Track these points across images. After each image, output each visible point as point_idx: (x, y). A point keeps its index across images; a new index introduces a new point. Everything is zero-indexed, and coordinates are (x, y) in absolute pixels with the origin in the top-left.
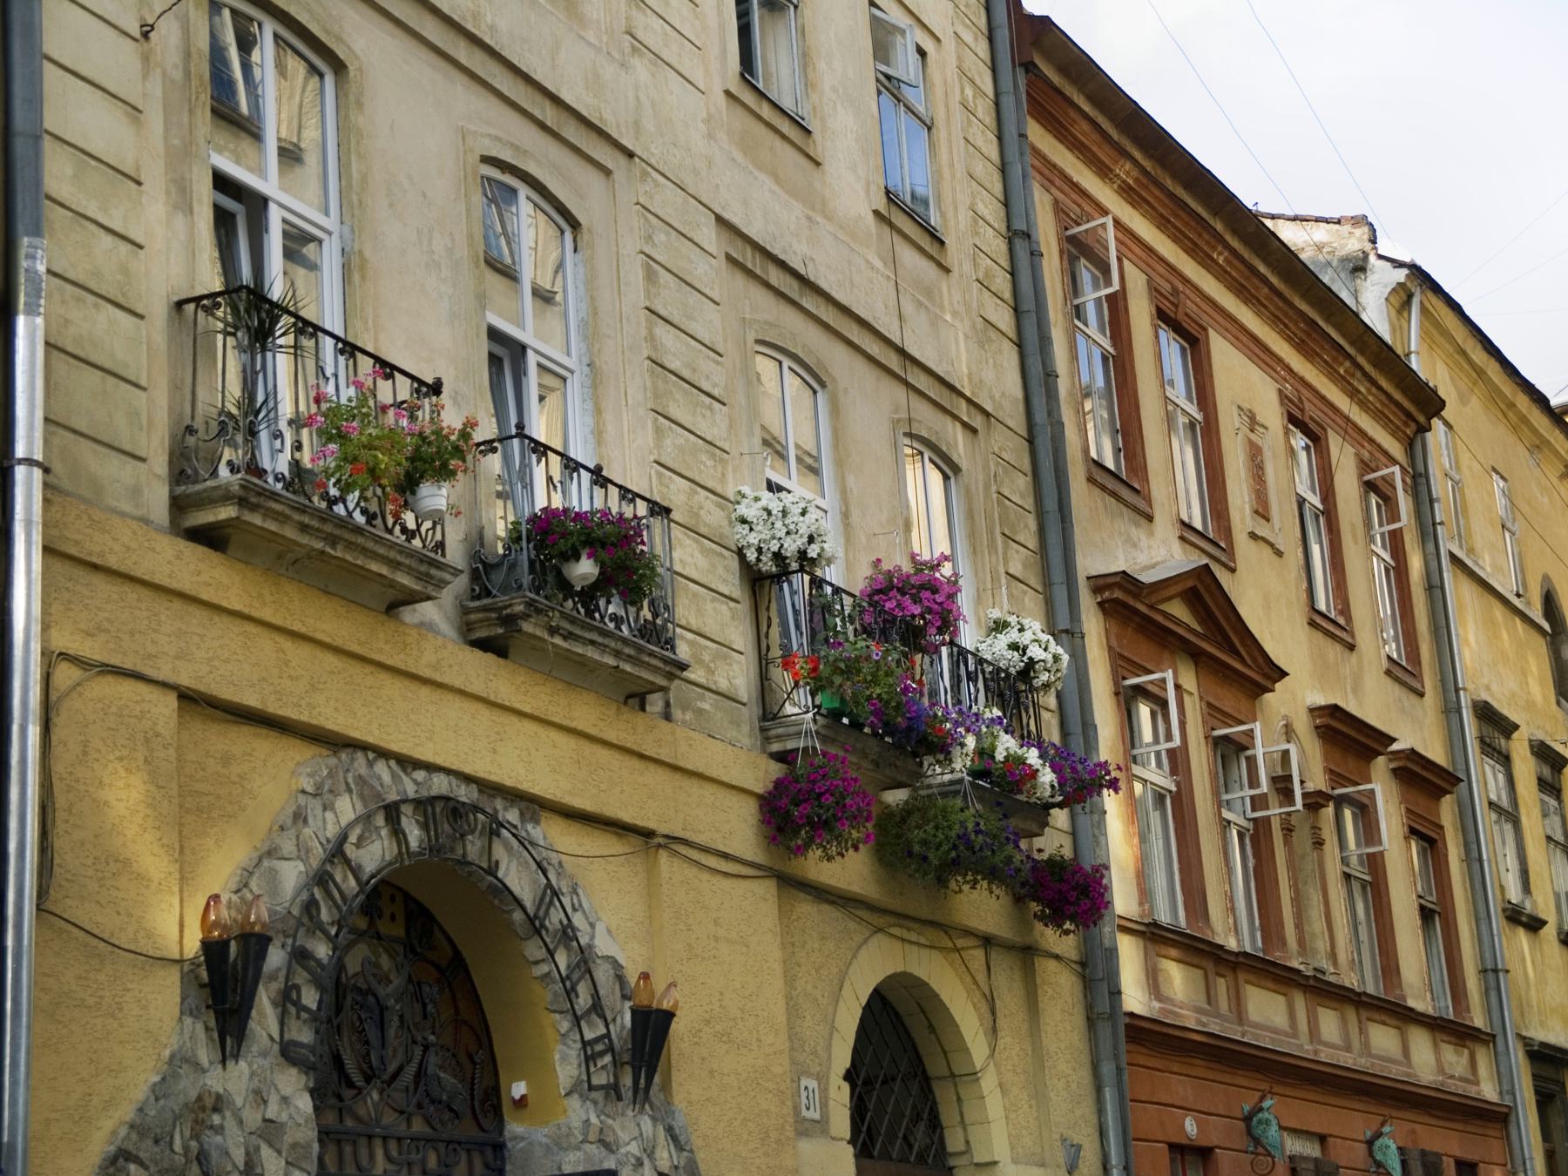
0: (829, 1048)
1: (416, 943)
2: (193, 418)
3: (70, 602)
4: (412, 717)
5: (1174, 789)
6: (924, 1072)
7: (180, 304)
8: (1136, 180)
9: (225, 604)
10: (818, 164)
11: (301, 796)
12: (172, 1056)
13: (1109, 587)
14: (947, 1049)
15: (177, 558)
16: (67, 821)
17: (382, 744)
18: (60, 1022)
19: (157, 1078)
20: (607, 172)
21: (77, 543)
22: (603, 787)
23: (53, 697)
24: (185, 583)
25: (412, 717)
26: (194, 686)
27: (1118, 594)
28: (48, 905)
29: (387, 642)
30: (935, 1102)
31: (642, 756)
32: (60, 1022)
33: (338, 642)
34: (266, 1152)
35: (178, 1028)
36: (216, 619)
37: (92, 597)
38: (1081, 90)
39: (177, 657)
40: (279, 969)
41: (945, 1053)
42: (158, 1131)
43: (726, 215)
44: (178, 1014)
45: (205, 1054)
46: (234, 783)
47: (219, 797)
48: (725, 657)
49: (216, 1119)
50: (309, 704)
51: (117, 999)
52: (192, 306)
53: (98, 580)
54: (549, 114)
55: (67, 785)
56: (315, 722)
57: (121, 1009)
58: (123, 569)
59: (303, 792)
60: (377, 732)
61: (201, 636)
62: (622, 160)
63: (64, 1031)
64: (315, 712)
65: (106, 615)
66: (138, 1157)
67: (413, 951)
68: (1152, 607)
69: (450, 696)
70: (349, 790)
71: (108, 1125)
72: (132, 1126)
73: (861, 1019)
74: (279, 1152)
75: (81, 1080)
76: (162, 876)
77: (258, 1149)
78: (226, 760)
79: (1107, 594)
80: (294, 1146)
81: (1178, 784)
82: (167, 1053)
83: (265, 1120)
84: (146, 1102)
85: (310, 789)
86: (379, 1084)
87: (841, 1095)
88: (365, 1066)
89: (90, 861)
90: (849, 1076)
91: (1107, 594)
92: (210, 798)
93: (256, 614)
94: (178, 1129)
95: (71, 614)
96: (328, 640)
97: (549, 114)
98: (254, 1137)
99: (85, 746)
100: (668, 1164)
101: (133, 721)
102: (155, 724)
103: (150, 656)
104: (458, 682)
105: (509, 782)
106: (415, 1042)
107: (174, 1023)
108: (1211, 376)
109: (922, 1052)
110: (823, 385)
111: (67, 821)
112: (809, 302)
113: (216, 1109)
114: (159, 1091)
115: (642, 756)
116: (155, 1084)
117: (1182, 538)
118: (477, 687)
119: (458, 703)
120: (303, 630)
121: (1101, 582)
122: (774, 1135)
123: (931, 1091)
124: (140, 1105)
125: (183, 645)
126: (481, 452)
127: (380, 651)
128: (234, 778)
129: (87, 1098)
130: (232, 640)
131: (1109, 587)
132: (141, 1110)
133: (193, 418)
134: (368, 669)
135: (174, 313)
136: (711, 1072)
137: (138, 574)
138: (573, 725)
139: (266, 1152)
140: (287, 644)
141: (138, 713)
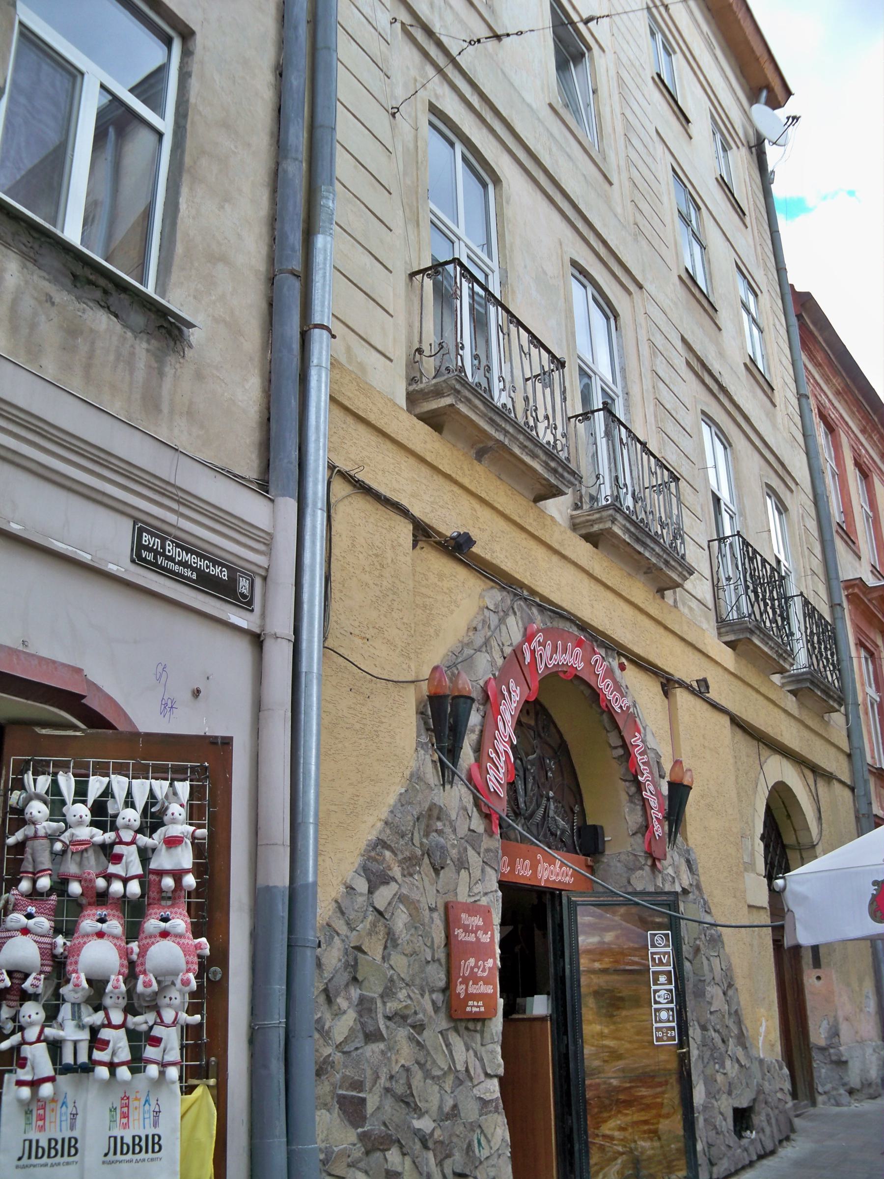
0: (753, 821)
1: (541, 730)
2: (420, 342)
3: (344, 438)
4: (549, 573)
5: (878, 699)
6: (782, 842)
7: (413, 275)
8: (843, 389)
9: (440, 467)
10: (720, 329)
11: (485, 610)
12: (412, 775)
13: (852, 586)
14: (796, 828)
15: (413, 428)
16: (341, 592)
17: (532, 586)
18: (337, 738)
19: (403, 790)
20: (629, 293)
21: (350, 398)
22: (648, 642)
23: (333, 501)
24: (418, 448)
25: (549, 573)
26: (422, 518)
27: (856, 591)
28: (330, 643)
29: (535, 520)
30: (787, 860)
31: (666, 628)
32: (337, 738)
33: (507, 512)
34: (471, 852)
35: (415, 755)
36: (435, 477)
37: (358, 439)
38: (821, 335)
39: (412, 496)
40: (475, 725)
41: (795, 830)
42: (403, 828)
43: (686, 336)
44: (415, 745)
45: (431, 775)
46: (446, 593)
47: (436, 600)
48: (701, 580)
49: (439, 825)
50: (490, 549)
51: (375, 728)
52: (419, 277)
53: (362, 429)
54: (602, 251)
55: (342, 566)
56: (494, 562)
57: (378, 736)
58: (378, 425)
59: (487, 608)
60: (529, 578)
61: (427, 486)
62: (637, 289)
63: (340, 745)
64: (495, 555)
65: (368, 454)
66: (390, 846)
67: (539, 736)
68: (869, 600)
69: (569, 565)
70: (515, 614)
71: (371, 820)
72: (386, 823)
73: (795, 796)
74: (479, 854)
75: (351, 784)
76: (404, 645)
77: (466, 850)
78: (441, 577)
79: (850, 590)
80: (488, 850)
81: (880, 697)
82: (407, 773)
83: (470, 830)
84: (395, 806)
85: (492, 607)
86: (523, 821)
87: (760, 847)
88: (515, 808)
89: (356, 624)
90: (762, 838)
91: (850, 590)
92: (431, 600)
93: (460, 479)
94: (416, 828)
95: (345, 446)
96: (501, 509)
97: (602, 251)
98: (463, 841)
99: (354, 541)
100: (688, 883)
101: (384, 531)
102: (399, 537)
103: (394, 490)
104: (573, 556)
105: (600, 628)
106: (542, 796)
107: (412, 751)
108: (875, 495)
109: (781, 831)
110: (730, 445)
111: (341, 592)
112: (722, 397)
113: (439, 819)
114: (404, 801)
115: (666, 628)
116: (401, 794)
117: (872, 571)
118: (583, 562)
119: (572, 570)
120: (487, 498)
121: (849, 583)
122: (735, 869)
123: (786, 854)
124: (392, 808)
125: (415, 488)
126: (579, 420)
127: (530, 524)
128: (445, 590)
129: (356, 798)
130: (444, 493)
131: (852, 586)
132: (392, 812)
133: (420, 342)
134: (524, 535)
135: (408, 280)
136: (705, 827)
137: (388, 431)
138: (633, 599)
139: (471, 852)
140: (476, 505)
141: (387, 526)
